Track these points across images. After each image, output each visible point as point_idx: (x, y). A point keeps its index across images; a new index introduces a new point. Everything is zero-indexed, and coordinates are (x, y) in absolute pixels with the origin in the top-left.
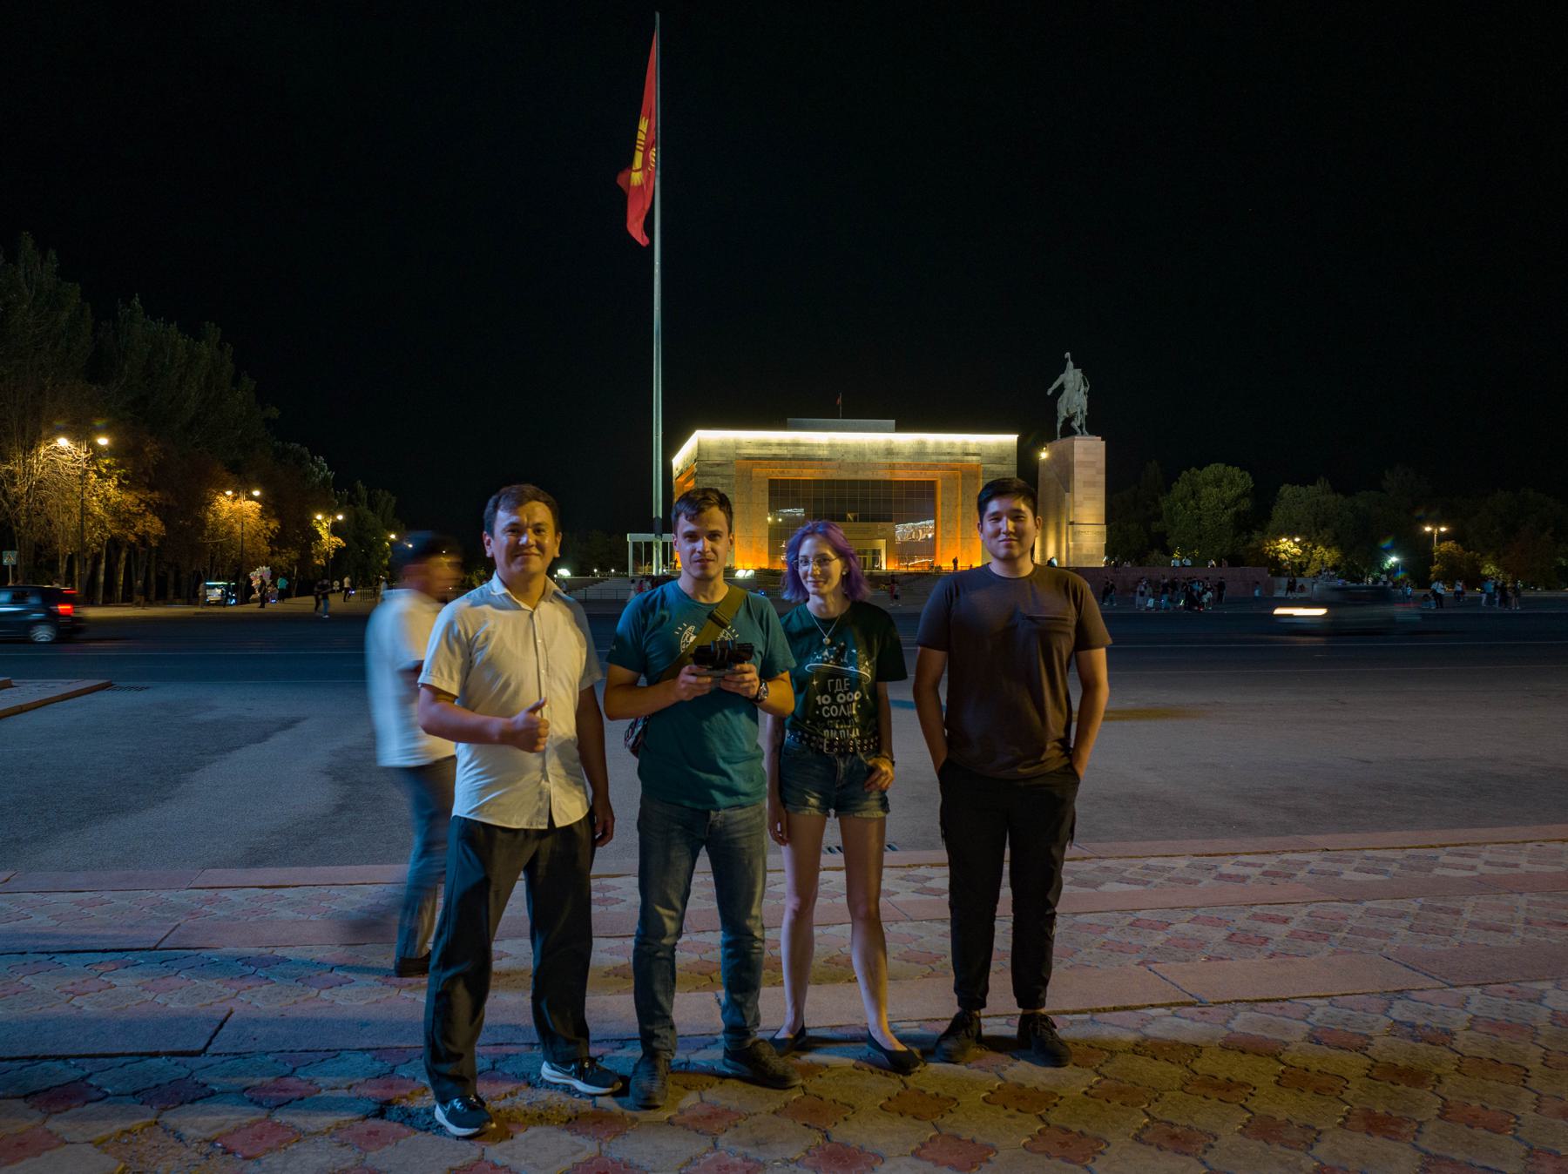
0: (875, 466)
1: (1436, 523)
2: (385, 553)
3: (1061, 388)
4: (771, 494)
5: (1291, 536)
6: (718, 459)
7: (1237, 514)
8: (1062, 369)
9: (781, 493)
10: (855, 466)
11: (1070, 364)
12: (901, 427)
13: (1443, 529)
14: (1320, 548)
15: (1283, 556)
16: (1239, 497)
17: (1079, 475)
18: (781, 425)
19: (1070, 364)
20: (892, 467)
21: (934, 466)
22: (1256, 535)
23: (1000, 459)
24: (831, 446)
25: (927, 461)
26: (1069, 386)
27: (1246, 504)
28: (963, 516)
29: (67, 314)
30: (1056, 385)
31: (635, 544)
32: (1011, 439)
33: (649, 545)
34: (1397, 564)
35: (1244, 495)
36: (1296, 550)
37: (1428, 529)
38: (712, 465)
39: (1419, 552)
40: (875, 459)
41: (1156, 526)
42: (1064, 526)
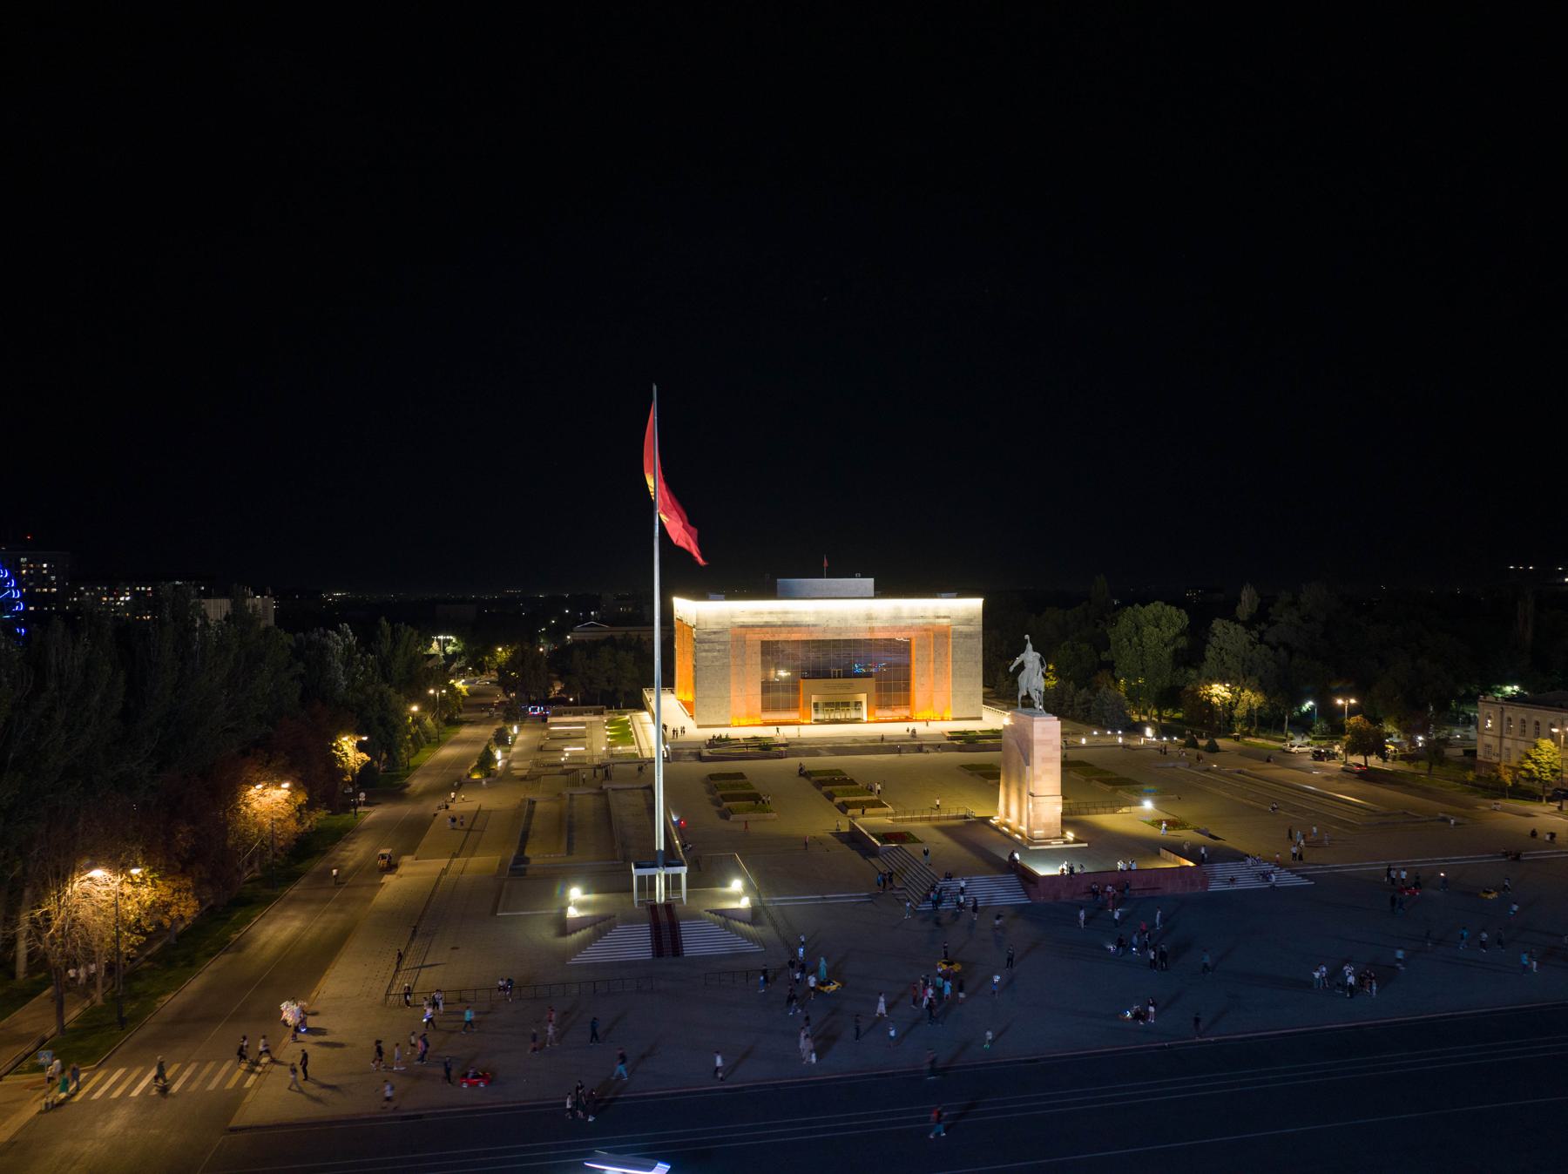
0: (857, 630)
1: (1346, 696)
2: (408, 727)
3: (1021, 667)
4: (763, 653)
5: (1223, 682)
6: (716, 628)
7: (1176, 650)
8: (1023, 650)
9: (771, 651)
10: (839, 630)
11: (1030, 646)
12: (882, 591)
13: (1353, 701)
14: (1247, 692)
15: (1215, 700)
16: (1175, 639)
17: (1038, 752)
18: (770, 592)
19: (1030, 646)
20: (872, 629)
21: (910, 628)
22: (1193, 673)
23: (968, 621)
24: (817, 613)
25: (903, 624)
26: (1028, 666)
27: (1183, 642)
28: (936, 670)
29: (97, 697)
30: (1018, 660)
31: (639, 878)
32: (975, 605)
33: (652, 878)
34: (1312, 708)
35: (1182, 633)
36: (1228, 695)
37: (1340, 702)
38: (709, 633)
39: (1336, 974)
40: (856, 623)
41: (1105, 656)
42: (1025, 796)
